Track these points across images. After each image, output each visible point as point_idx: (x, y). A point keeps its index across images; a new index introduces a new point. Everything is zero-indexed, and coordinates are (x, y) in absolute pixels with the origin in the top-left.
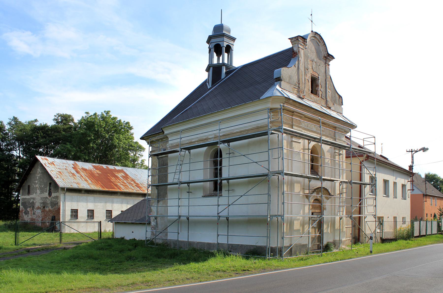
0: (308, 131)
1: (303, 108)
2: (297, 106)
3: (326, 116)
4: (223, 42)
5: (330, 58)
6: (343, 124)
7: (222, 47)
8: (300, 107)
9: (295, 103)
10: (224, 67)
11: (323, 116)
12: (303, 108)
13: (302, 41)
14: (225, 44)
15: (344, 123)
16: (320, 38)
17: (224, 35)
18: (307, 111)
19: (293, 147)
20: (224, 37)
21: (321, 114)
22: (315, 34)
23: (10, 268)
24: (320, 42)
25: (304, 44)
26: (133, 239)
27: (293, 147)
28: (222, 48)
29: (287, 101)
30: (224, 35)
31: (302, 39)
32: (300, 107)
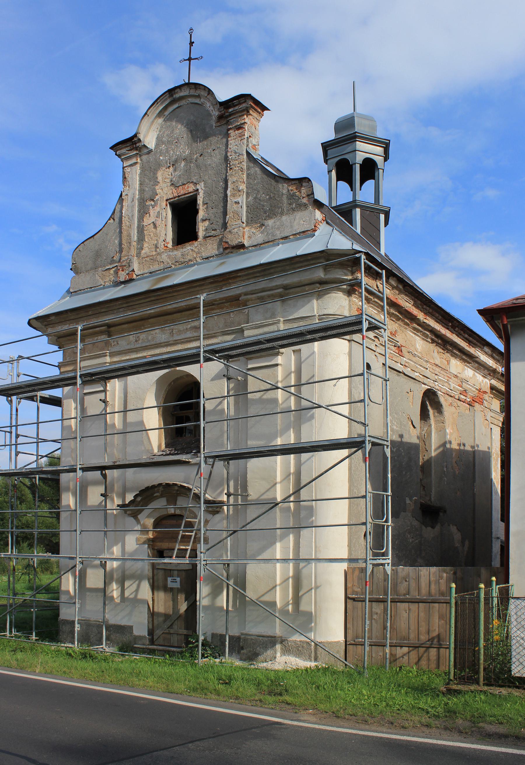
0: (132, 352)
1: (90, 313)
2: (72, 317)
3: (166, 293)
4: (354, 153)
5: (237, 108)
6: (258, 275)
7: (352, 165)
8: (80, 316)
9: (64, 316)
10: (358, 210)
11: (159, 298)
12: (90, 313)
13: (128, 148)
14: (360, 157)
15: (265, 270)
16: (193, 86)
17: (356, 137)
18: (106, 313)
19: (86, 407)
20: (357, 142)
21: (150, 297)
22: (172, 96)
23: (201, 638)
24: (199, 96)
25: (136, 149)
26: (508, 608)
27: (86, 407)
28: (354, 166)
29: (46, 322)
30: (356, 137)
31: (124, 146)
32: (80, 316)
